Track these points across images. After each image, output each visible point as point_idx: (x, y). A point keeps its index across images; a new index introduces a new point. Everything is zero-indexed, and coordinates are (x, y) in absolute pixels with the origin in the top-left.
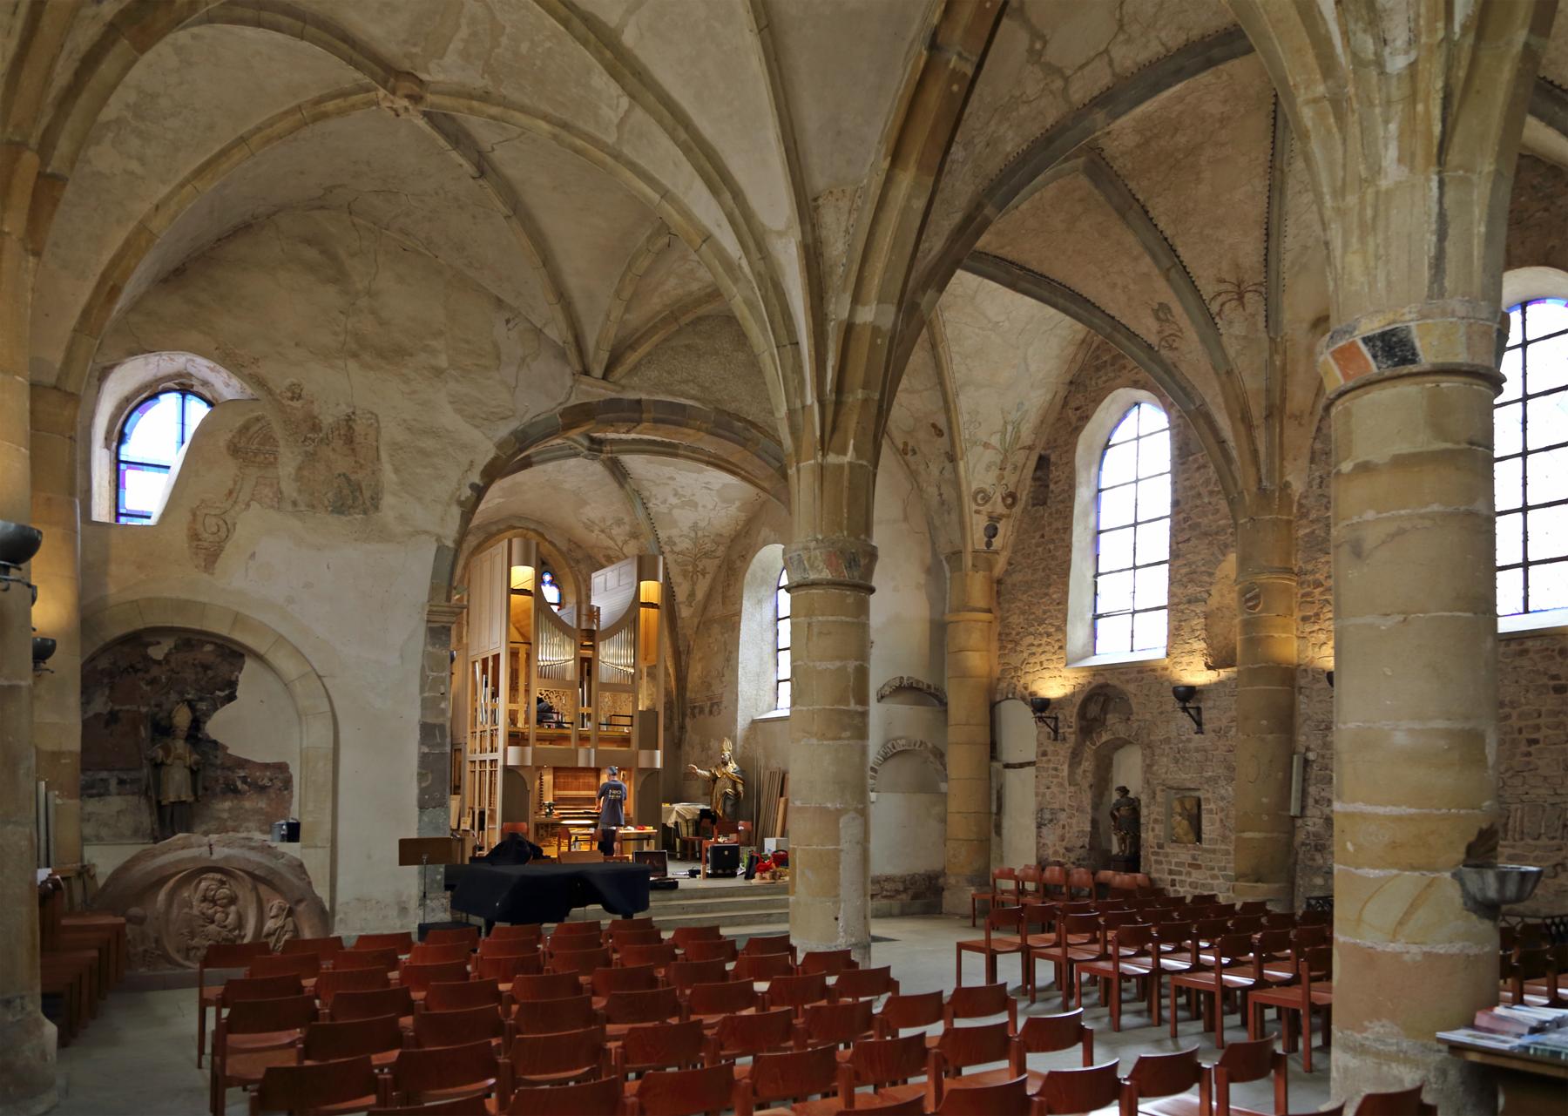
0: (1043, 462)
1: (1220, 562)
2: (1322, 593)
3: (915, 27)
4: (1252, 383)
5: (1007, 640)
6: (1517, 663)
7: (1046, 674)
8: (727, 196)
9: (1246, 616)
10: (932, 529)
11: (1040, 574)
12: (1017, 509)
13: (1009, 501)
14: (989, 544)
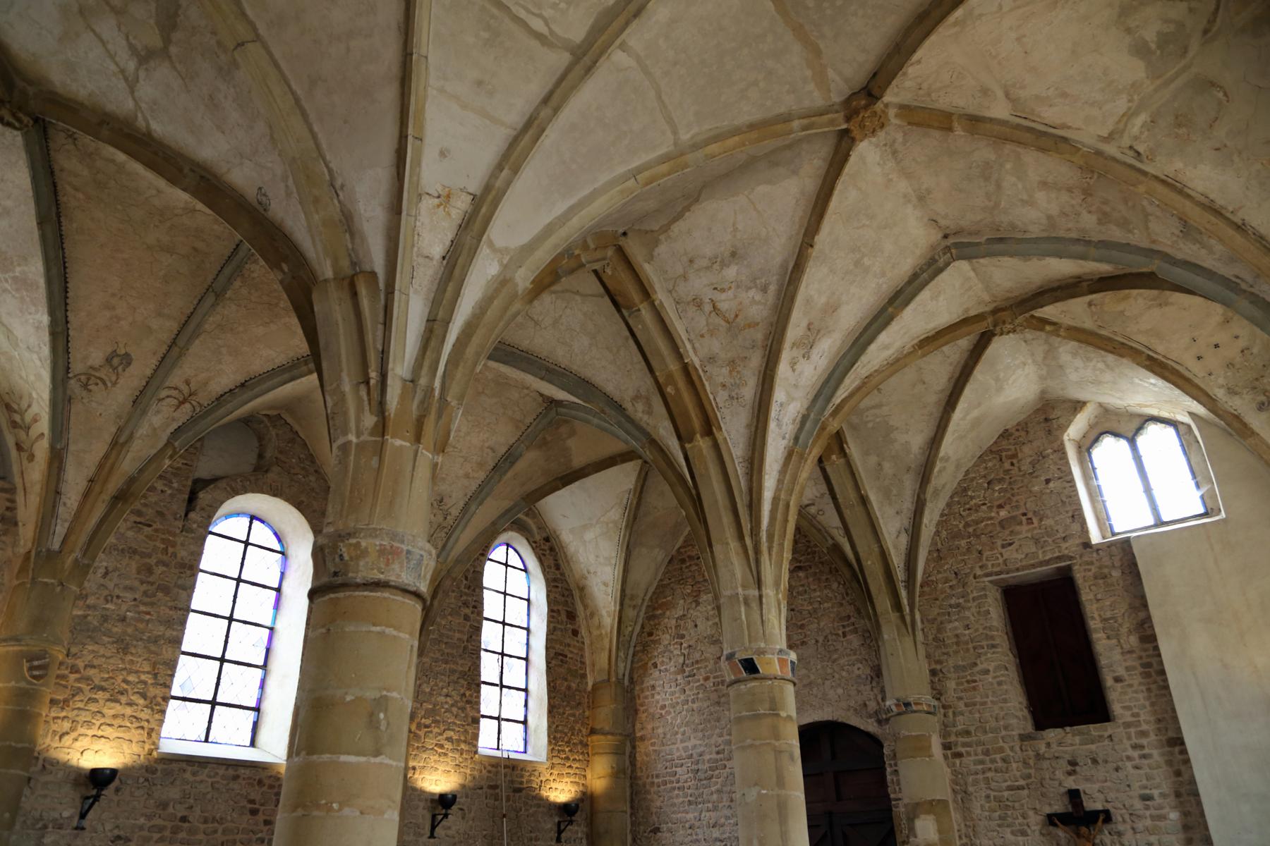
2: (78, 680)
6: (231, 785)
9: (23, 685)
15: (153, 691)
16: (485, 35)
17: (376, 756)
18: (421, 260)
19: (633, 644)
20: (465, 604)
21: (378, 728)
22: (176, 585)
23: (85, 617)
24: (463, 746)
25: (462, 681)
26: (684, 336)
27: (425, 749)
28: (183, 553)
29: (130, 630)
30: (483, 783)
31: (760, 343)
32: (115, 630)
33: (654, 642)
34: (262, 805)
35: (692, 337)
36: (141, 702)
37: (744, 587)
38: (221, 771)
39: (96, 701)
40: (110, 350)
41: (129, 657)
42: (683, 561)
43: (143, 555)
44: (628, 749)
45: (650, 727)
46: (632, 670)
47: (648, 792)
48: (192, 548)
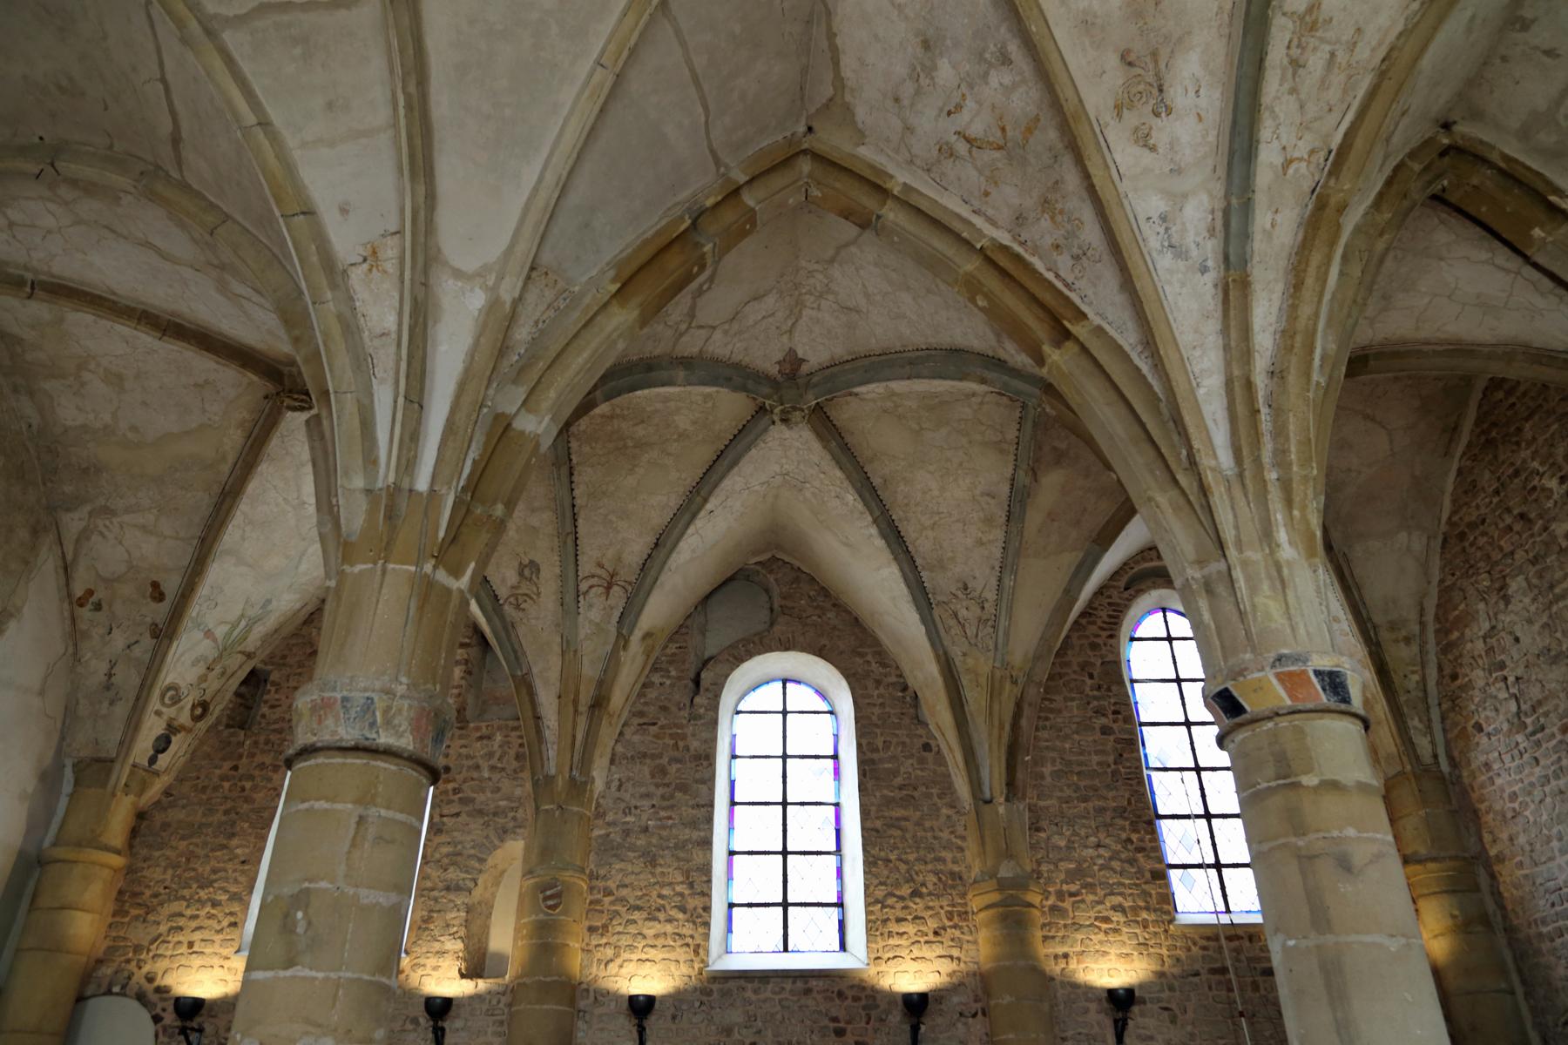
0: (255, 680)
1: (496, 848)
2: (612, 903)
3: (685, 194)
4: (590, 670)
5: (131, 899)
6: (803, 1002)
7: (196, 961)
8: (421, 190)
9: (541, 916)
10: (70, 712)
11: (219, 817)
12: (203, 725)
13: (199, 711)
14: (153, 760)
15: (693, 903)
16: (298, 51)
17: (286, 968)
18: (377, 342)
19: (1433, 701)
20: (1099, 712)
21: (293, 932)
22: (697, 781)
23: (608, 835)
24: (1144, 915)
25: (1119, 822)
26: (964, 211)
27: (1077, 927)
28: (695, 744)
29: (654, 841)
30: (1197, 967)
31: (1060, 146)
32: (639, 843)
33: (1463, 688)
34: (848, 1022)
35: (977, 204)
36: (681, 916)
37: (1201, 562)
38: (788, 985)
39: (635, 922)
40: (516, 564)
41: (659, 870)
42: (1462, 536)
43: (653, 757)
44: (1484, 881)
45: (1505, 836)
46: (1447, 743)
47: (1539, 952)
48: (705, 735)
